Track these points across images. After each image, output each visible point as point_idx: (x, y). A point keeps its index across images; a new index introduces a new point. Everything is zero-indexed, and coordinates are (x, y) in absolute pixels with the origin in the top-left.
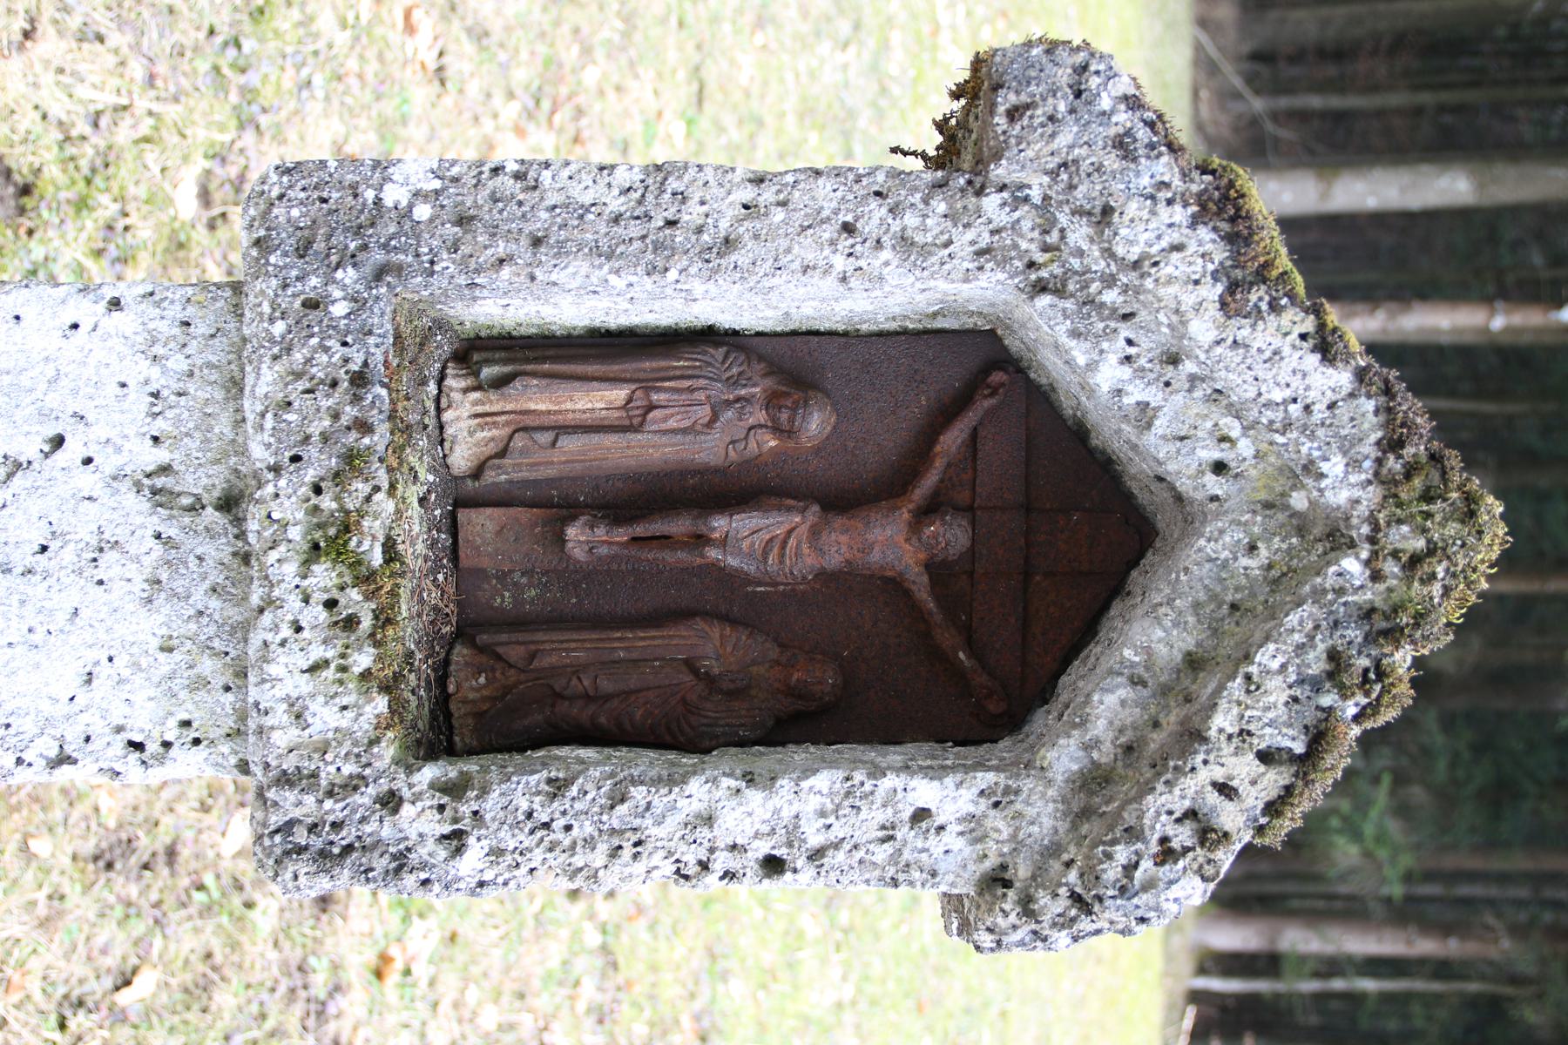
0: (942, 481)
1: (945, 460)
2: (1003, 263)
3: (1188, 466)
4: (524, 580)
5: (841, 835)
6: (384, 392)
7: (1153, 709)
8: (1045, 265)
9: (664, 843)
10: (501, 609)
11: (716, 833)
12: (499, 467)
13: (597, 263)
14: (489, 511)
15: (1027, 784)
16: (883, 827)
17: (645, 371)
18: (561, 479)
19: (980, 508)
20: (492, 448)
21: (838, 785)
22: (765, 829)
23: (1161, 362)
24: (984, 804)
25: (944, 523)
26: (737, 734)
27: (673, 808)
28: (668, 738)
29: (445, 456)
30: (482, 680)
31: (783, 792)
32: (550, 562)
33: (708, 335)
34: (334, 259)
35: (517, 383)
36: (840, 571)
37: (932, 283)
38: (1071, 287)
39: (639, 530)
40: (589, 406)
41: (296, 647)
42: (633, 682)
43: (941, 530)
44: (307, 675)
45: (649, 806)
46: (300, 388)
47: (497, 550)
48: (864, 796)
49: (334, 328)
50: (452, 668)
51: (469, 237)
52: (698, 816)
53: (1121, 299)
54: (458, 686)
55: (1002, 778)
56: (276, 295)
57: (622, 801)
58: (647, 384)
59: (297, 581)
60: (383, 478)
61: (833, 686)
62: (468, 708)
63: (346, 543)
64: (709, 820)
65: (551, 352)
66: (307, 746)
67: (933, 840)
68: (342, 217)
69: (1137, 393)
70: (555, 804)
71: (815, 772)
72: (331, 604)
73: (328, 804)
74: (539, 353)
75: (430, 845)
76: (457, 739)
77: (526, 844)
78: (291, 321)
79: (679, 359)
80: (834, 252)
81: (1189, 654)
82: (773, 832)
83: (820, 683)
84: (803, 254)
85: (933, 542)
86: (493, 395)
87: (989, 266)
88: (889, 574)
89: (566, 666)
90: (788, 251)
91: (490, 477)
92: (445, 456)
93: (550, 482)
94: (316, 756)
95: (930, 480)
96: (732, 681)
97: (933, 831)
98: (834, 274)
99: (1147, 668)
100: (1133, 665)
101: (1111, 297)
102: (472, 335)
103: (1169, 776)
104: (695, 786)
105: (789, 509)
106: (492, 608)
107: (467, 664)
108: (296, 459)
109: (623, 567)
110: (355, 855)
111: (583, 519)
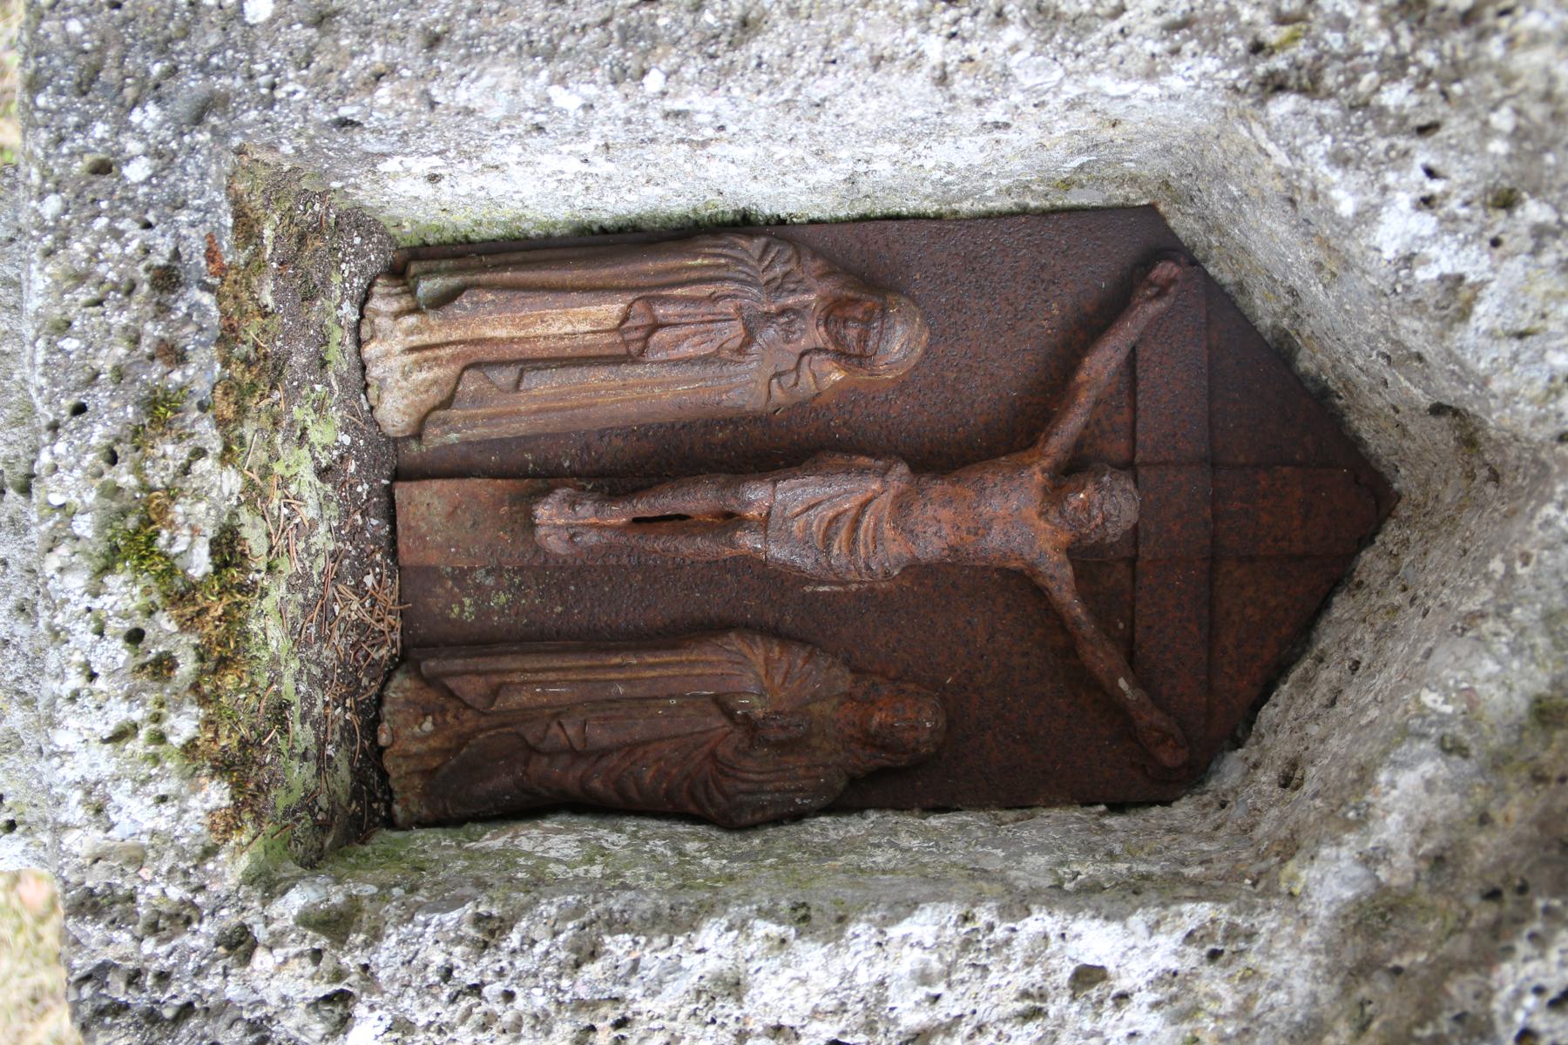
0: (1087, 426)
1: (1093, 393)
2: (1213, 42)
3: (1530, 382)
4: (490, 581)
5: (955, 1012)
6: (207, 299)
7: (1479, 795)
8: (1282, 46)
9: (665, 1022)
10: (459, 622)
11: (747, 1009)
12: (445, 422)
13: (529, 67)
14: (436, 484)
15: (1267, 923)
16: (1025, 995)
17: (646, 274)
18: (537, 437)
19: (1145, 464)
20: (435, 396)
21: (950, 931)
22: (829, 1003)
23: (1485, 205)
24: (1194, 955)
25: (1100, 488)
26: (792, 802)
27: (675, 968)
28: (692, 808)
29: (372, 408)
30: (428, 726)
31: (858, 945)
32: (522, 555)
33: (744, 224)
34: (129, 93)
35: (465, 300)
36: (941, 563)
37: (1092, 81)
38: (1330, 80)
39: (642, 507)
40: (569, 329)
41: (90, 703)
42: (639, 730)
43: (1097, 498)
44: (108, 746)
45: (635, 967)
46: (83, 298)
47: (448, 540)
48: (996, 948)
49: (130, 201)
50: (386, 709)
51: (328, 40)
52: (718, 979)
53: (1414, 100)
54: (395, 735)
55: (1223, 913)
56: (47, 156)
57: (593, 956)
58: (650, 293)
59: (87, 601)
60: (213, 441)
61: (933, 731)
62: (412, 765)
63: (151, 540)
64: (735, 987)
65: (518, 257)
66: (118, 854)
67: (1109, 1017)
68: (141, 27)
69: (1445, 259)
70: (485, 961)
71: (912, 906)
72: (135, 637)
73: (149, 946)
74: (502, 258)
75: (299, 1014)
76: (397, 808)
77: (445, 1017)
78: (67, 194)
79: (696, 257)
80: (926, 31)
81: (1538, 700)
82: (842, 1008)
83: (913, 728)
84: (871, 35)
85: (1083, 516)
86: (433, 319)
87: (1192, 45)
88: (1014, 565)
89: (543, 707)
90: (847, 32)
91: (436, 438)
92: (372, 408)
93: (522, 441)
94: (130, 870)
95: (1072, 425)
96: (783, 728)
97: (1109, 1003)
98: (926, 70)
99: (1469, 725)
100: (1443, 720)
101: (1395, 96)
102: (416, 242)
103: (1537, 926)
104: (711, 934)
105: (862, 471)
106: (448, 620)
107: (408, 702)
108: (79, 409)
109: (625, 561)
110: (194, 1022)
111: (561, 493)
